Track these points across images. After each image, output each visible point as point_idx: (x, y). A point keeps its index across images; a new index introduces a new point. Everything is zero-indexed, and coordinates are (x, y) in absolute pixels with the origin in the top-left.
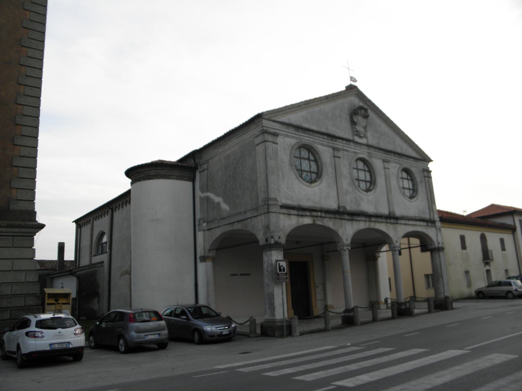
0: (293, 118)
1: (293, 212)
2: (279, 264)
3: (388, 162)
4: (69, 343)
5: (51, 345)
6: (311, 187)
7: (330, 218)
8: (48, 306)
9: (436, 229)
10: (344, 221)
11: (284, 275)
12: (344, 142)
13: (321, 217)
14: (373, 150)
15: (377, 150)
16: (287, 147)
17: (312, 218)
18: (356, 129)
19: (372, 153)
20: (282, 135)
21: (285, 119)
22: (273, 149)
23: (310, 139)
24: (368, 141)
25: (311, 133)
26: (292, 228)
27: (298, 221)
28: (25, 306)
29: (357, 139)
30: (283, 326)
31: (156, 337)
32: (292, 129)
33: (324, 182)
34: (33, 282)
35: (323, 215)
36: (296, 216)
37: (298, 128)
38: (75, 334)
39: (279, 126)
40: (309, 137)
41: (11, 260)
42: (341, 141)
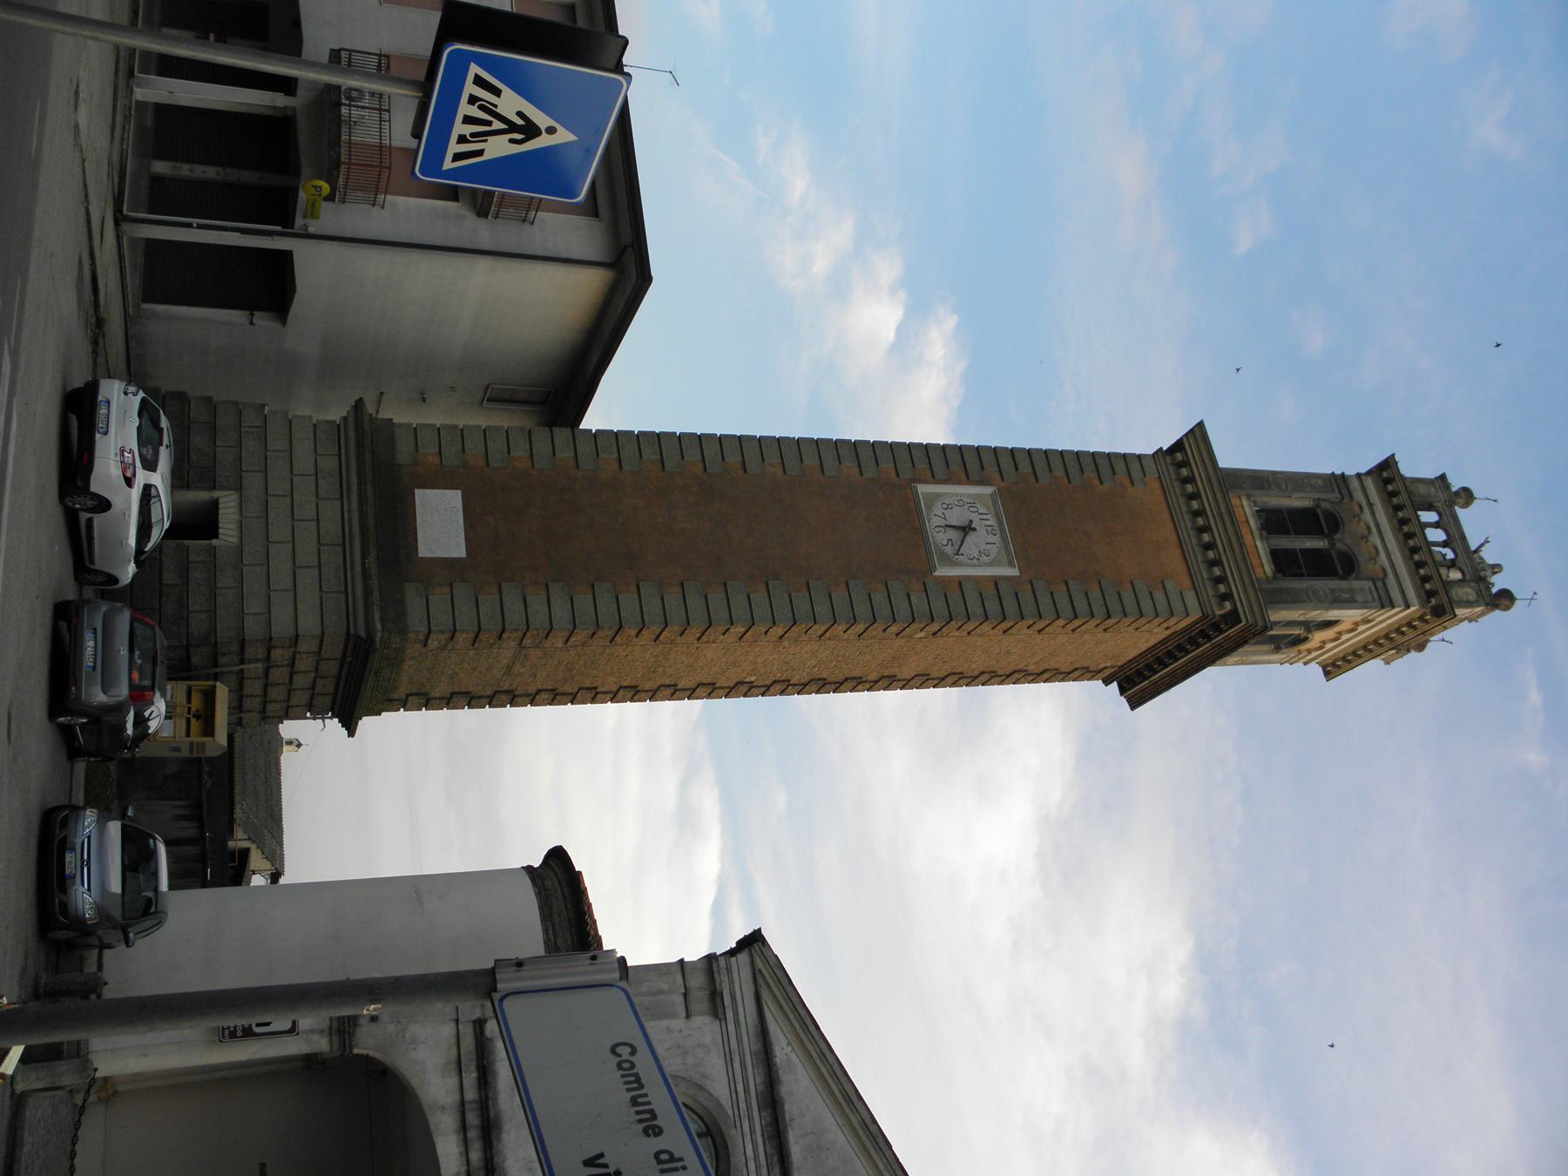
0: (798, 1086)
1: (471, 1077)
4: (106, 433)
5: (108, 402)
8: (185, 687)
16: (690, 1060)
21: (784, 1049)
22: (660, 992)
23: (752, 1165)
26: (414, 1082)
27: (443, 1108)
28: (188, 611)
32: (758, 1080)
34: (243, 627)
36: (457, 1098)
37: (772, 1101)
38: (122, 451)
39: (749, 1024)
40: (756, 1156)
41: (291, 587)
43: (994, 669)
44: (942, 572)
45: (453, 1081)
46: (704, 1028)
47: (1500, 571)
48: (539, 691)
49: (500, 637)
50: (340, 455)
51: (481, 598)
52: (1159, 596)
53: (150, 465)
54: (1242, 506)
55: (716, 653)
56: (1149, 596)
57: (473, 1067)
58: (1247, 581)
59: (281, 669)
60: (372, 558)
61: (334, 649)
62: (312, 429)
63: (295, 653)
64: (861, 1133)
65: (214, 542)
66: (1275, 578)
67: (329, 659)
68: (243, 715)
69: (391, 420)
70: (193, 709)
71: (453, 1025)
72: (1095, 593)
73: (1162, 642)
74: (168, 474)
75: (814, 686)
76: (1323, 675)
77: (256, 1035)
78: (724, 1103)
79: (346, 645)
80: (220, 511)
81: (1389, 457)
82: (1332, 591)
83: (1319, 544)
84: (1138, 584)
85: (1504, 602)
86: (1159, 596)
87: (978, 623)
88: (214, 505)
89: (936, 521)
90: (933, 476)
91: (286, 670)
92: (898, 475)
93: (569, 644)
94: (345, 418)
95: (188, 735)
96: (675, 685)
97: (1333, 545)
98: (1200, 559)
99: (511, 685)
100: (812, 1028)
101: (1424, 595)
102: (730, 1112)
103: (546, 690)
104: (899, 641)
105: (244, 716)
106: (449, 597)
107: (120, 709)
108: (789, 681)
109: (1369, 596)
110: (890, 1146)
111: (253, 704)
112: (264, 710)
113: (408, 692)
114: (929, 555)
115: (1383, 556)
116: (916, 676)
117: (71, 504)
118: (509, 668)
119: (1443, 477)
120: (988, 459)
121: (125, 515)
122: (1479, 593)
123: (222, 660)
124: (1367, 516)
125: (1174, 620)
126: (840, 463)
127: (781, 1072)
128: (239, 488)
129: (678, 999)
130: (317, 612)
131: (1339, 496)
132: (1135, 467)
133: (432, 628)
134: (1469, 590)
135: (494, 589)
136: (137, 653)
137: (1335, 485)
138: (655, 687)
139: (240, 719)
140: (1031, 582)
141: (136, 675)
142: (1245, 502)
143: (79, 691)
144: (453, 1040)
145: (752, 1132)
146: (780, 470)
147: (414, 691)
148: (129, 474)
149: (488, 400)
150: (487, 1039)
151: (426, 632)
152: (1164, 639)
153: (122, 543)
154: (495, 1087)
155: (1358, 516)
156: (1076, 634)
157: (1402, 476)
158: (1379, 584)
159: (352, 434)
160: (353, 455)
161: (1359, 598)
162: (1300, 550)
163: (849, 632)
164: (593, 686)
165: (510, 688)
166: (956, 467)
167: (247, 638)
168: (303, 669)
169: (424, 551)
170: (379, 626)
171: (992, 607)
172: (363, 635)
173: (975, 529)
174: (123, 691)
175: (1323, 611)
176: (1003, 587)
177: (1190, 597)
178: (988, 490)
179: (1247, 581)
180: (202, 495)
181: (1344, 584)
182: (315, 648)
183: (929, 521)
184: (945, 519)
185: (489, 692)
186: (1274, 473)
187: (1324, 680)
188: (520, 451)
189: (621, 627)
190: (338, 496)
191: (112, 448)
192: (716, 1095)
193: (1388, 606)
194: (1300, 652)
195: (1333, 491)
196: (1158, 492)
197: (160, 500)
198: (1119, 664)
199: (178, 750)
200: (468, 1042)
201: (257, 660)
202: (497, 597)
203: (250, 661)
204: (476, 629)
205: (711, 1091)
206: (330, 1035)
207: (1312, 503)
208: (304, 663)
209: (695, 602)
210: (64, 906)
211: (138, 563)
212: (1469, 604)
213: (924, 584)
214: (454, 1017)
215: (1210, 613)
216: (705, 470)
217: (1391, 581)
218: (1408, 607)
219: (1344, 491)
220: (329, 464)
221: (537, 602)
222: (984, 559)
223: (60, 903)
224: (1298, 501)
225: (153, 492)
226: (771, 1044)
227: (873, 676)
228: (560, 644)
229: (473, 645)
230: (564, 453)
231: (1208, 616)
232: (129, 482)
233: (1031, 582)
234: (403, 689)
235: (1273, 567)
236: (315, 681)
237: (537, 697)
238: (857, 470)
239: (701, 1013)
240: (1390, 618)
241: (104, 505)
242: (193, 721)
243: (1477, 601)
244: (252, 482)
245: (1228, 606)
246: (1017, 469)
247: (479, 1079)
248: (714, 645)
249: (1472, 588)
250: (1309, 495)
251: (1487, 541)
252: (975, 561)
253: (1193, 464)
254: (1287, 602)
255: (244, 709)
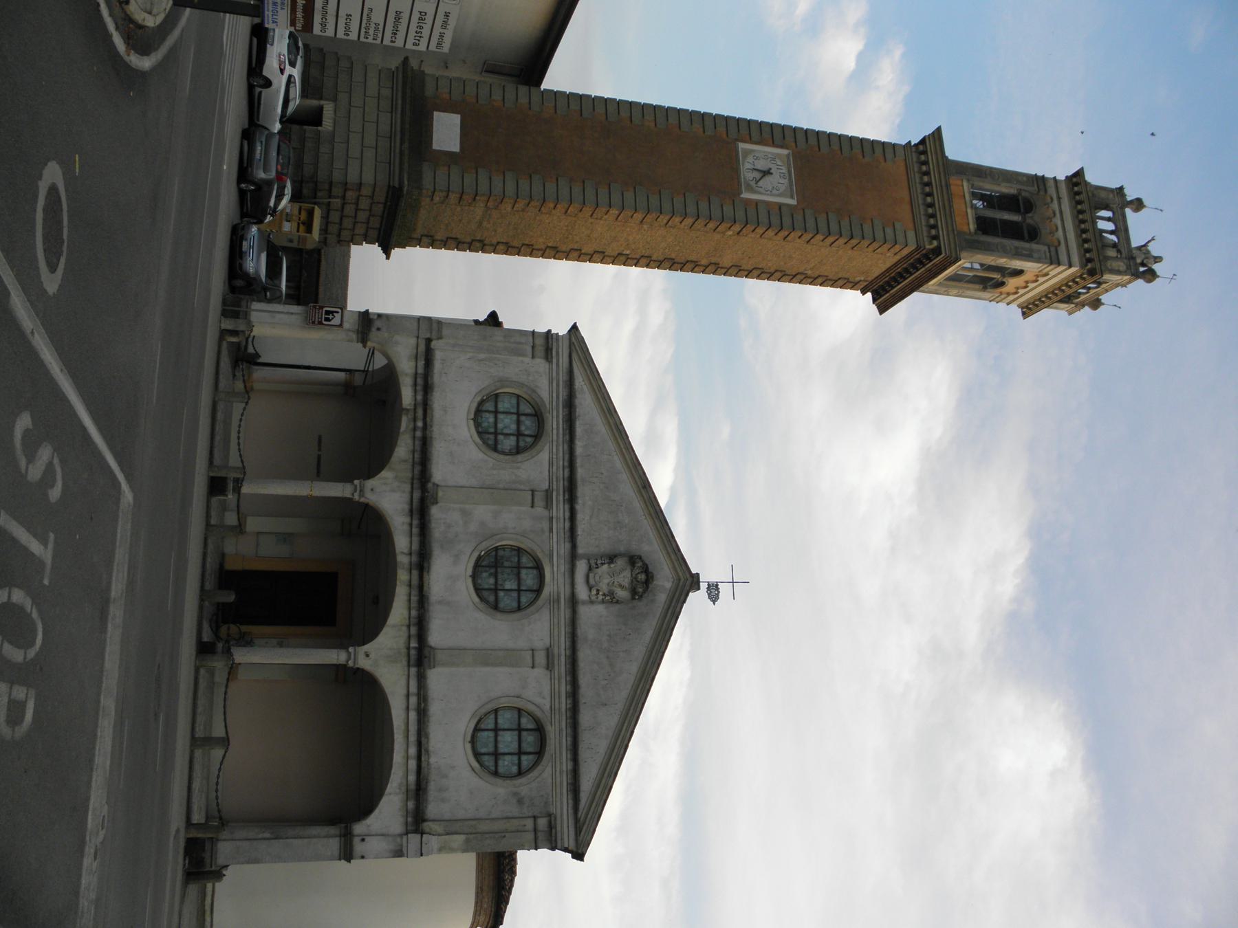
0: (585, 401)
1: (421, 363)
2: (337, 312)
3: (549, 666)
4: (272, 45)
6: (468, 419)
7: (413, 452)
8: (298, 207)
9: (401, 835)
10: (407, 487)
11: (319, 318)
12: (567, 525)
13: (415, 429)
14: (569, 743)
15: (569, 629)
16: (531, 378)
17: (412, 407)
18: (602, 564)
19: (559, 608)
20: (551, 369)
21: (580, 382)
22: (520, 343)
23: (555, 432)
24: (584, 603)
25: (567, 437)
27: (406, 375)
29: (581, 567)
30: (239, 306)
31: (258, 156)
33: (481, 455)
35: (419, 434)
37: (570, 404)
42: (567, 514)
43: (784, 269)
44: (746, 195)
45: (412, 364)
46: (540, 364)
47: (1160, 262)
48: (498, 243)
49: (474, 199)
50: (393, 88)
51: (466, 175)
52: (889, 231)
53: (293, 64)
54: (963, 186)
55: (603, 227)
56: (882, 230)
57: (423, 358)
58: (950, 229)
59: (351, 205)
60: (406, 145)
61: (381, 196)
62: (378, 72)
63: (359, 196)
64: (613, 427)
65: (320, 128)
66: (975, 233)
67: (378, 203)
68: (328, 236)
69: (558, 333)
70: (302, 219)
71: (415, 339)
72: (845, 222)
73: (895, 265)
74: (301, 71)
75: (667, 264)
76: (1021, 314)
77: (323, 324)
78: (545, 399)
79: (388, 193)
80: (324, 112)
81: (1080, 169)
82: (1017, 248)
83: (1015, 218)
84: (876, 222)
85: (1149, 276)
86: (889, 231)
87: (765, 229)
88: (321, 109)
89: (748, 166)
90: (751, 139)
91: (353, 207)
92: (727, 136)
93: (515, 209)
94: (397, 68)
95: (298, 231)
96: (580, 250)
97: (1024, 219)
98: (922, 213)
99: (482, 236)
100: (596, 374)
101: (1084, 261)
102: (548, 406)
103: (503, 243)
104: (717, 236)
105: (328, 236)
106: (447, 172)
107: (269, 183)
108: (651, 257)
109: (1044, 256)
110: (628, 437)
111: (333, 229)
112: (339, 235)
113: (422, 233)
114: (739, 185)
115: (1060, 232)
116: (732, 266)
117: (252, 82)
118: (480, 223)
119: (1121, 189)
120: (788, 134)
121: (278, 91)
122: (1129, 267)
123: (319, 194)
124: (1055, 206)
125: (898, 247)
126: (692, 124)
127: (577, 393)
128: (335, 99)
129: (529, 349)
130: (373, 171)
131: (1037, 189)
132: (889, 151)
133: (437, 188)
134: (1122, 264)
135: (474, 171)
136: (280, 157)
137: (1035, 182)
138: (568, 250)
139: (326, 239)
140: (804, 210)
141: (279, 167)
142: (965, 184)
143: (252, 170)
144: (415, 346)
145: (558, 416)
146: (653, 124)
147: (426, 233)
148: (282, 67)
149: (486, 71)
150: (431, 349)
151: (433, 190)
152: (897, 263)
153: (275, 109)
154: (433, 371)
155: (1048, 204)
156: (834, 249)
157: (1086, 181)
158: (1053, 249)
159: (400, 76)
160: (400, 88)
161: (1035, 255)
162: (1000, 220)
163: (683, 223)
164: (530, 243)
165: (482, 239)
166: (767, 135)
167: (333, 181)
168: (362, 208)
169: (435, 146)
170: (406, 183)
171: (775, 220)
172: (397, 185)
173: (772, 174)
174: (273, 175)
175: (1009, 260)
176: (784, 209)
177: (911, 235)
178: (785, 152)
179: (950, 229)
180: (315, 103)
181: (1027, 245)
182: (370, 194)
183: (743, 165)
184: (754, 165)
185: (468, 240)
186: (991, 169)
187: (1022, 318)
188: (497, 96)
189: (544, 201)
190: (390, 110)
191: (275, 54)
192: (542, 396)
193: (1056, 264)
194: (1001, 293)
195: (1033, 186)
196: (902, 168)
197: (296, 86)
198: (870, 279)
199: (291, 241)
200: (422, 348)
201: (338, 197)
202: (475, 175)
203: (335, 197)
204: (461, 192)
205: (539, 393)
206: (358, 333)
207: (1016, 191)
208: (364, 204)
209: (590, 193)
210: (241, 265)
211: (281, 122)
212: (1118, 272)
213: (733, 201)
214: (417, 335)
215: (922, 245)
216: (607, 118)
217: (1062, 249)
218: (1070, 266)
219: (1042, 187)
220: (386, 92)
221: (497, 181)
222: (775, 192)
223: (240, 263)
224: (1006, 189)
225: (292, 79)
226: (574, 379)
227: (704, 262)
228: (509, 209)
229: (459, 203)
230: (523, 100)
231: (920, 248)
232: (282, 71)
233: (804, 210)
234: (420, 230)
235: (976, 226)
236: (369, 219)
237: (498, 247)
238: (702, 130)
239: (540, 358)
240: (1059, 273)
241: (268, 83)
242: (301, 225)
243: (1126, 272)
244: (343, 97)
245: (935, 243)
246: (807, 142)
247: (425, 364)
248: (602, 222)
249: (1124, 263)
250: (1015, 186)
251: (1153, 239)
252: (769, 192)
253: (929, 154)
254: (981, 249)
255: (329, 232)
